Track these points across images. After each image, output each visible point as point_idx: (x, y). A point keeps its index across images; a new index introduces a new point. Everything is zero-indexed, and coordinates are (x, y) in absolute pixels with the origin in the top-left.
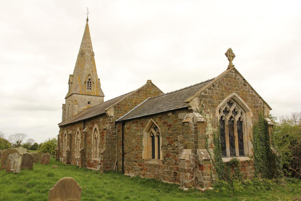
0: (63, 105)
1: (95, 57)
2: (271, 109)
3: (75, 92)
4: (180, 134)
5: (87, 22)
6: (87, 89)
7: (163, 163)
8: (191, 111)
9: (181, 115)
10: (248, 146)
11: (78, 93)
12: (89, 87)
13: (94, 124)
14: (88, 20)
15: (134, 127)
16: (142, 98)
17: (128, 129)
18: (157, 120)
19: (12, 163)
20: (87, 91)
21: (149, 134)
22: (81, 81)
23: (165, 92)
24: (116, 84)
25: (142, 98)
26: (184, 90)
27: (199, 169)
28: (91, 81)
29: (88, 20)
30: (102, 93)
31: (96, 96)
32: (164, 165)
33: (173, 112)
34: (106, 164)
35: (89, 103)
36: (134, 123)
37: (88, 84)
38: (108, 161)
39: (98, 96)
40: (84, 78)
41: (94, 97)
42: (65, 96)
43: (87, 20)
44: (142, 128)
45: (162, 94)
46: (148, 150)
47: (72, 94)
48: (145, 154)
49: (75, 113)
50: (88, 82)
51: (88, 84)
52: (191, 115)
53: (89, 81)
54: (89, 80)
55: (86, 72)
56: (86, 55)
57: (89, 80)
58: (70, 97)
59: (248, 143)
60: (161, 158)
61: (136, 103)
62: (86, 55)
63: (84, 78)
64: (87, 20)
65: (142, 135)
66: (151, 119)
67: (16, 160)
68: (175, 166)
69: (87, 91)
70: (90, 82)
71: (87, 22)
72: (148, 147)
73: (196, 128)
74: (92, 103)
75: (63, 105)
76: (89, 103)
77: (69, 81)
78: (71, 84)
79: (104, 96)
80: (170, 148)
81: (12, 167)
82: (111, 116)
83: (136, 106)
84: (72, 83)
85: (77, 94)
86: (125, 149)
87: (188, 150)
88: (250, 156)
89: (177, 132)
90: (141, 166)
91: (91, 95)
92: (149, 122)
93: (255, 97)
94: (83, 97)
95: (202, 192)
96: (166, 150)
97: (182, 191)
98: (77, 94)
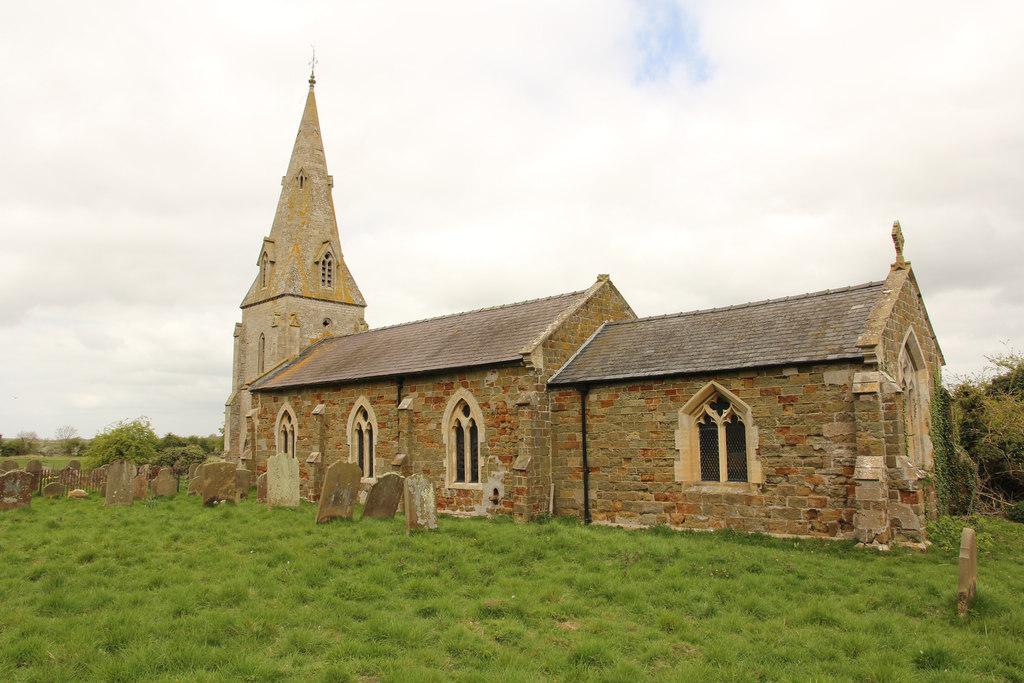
0: (238, 325)
1: (334, 192)
2: (944, 364)
3: (291, 291)
4: (831, 420)
5: (312, 86)
6: (321, 282)
7: (764, 491)
8: (873, 366)
9: (834, 376)
10: (923, 447)
11: (300, 293)
12: (327, 279)
13: (450, 387)
14: (315, 82)
15: (632, 400)
16: (594, 323)
17: (604, 404)
18: (737, 384)
19: (417, 502)
20: (323, 289)
21: (693, 420)
22: (302, 259)
23: (641, 315)
24: (412, 274)
25: (594, 323)
26: (762, 310)
27: (902, 501)
28: (330, 259)
29: (315, 82)
30: (360, 295)
31: (346, 304)
32: (766, 495)
33: (803, 367)
34: (533, 498)
35: (325, 324)
36: (631, 389)
37: (324, 269)
38: (537, 492)
39: (349, 304)
40: (304, 249)
41: (339, 306)
42: (240, 299)
43: (312, 82)
44: (671, 404)
45: (633, 319)
46: (691, 459)
47: (283, 295)
48: (686, 467)
49: (293, 353)
50: (324, 262)
51: (324, 269)
52: (871, 375)
53: (327, 261)
54: (327, 257)
55: (316, 232)
56: (308, 182)
57: (327, 257)
58: (270, 303)
59: (922, 440)
60: (756, 470)
61: (582, 335)
62: (308, 182)
63: (304, 249)
64: (312, 82)
65: (674, 422)
66: (713, 382)
67: (424, 494)
68: (812, 496)
69: (323, 289)
70: (330, 264)
71: (312, 86)
72: (691, 450)
73: (889, 408)
74: (335, 323)
75: (238, 325)
76: (325, 324)
77: (264, 254)
78: (269, 265)
79: (364, 306)
80: (789, 455)
81: (419, 514)
82: (538, 370)
83: (583, 341)
84: (273, 263)
85: (298, 296)
86: (590, 458)
87: (877, 458)
88: (926, 468)
89: (816, 416)
90: (666, 499)
91: (331, 302)
92: (702, 390)
93: (926, 334)
94: (312, 305)
95: (922, 551)
96: (776, 459)
97: (878, 553)
98: (298, 296)
